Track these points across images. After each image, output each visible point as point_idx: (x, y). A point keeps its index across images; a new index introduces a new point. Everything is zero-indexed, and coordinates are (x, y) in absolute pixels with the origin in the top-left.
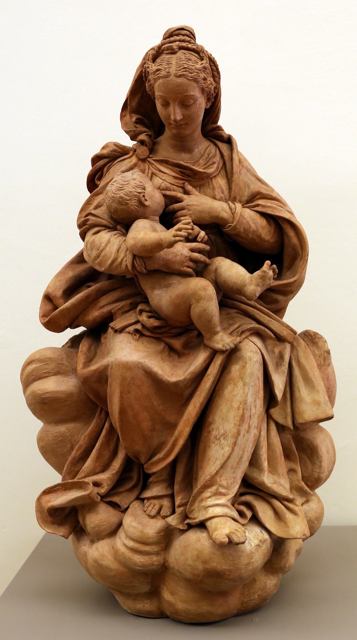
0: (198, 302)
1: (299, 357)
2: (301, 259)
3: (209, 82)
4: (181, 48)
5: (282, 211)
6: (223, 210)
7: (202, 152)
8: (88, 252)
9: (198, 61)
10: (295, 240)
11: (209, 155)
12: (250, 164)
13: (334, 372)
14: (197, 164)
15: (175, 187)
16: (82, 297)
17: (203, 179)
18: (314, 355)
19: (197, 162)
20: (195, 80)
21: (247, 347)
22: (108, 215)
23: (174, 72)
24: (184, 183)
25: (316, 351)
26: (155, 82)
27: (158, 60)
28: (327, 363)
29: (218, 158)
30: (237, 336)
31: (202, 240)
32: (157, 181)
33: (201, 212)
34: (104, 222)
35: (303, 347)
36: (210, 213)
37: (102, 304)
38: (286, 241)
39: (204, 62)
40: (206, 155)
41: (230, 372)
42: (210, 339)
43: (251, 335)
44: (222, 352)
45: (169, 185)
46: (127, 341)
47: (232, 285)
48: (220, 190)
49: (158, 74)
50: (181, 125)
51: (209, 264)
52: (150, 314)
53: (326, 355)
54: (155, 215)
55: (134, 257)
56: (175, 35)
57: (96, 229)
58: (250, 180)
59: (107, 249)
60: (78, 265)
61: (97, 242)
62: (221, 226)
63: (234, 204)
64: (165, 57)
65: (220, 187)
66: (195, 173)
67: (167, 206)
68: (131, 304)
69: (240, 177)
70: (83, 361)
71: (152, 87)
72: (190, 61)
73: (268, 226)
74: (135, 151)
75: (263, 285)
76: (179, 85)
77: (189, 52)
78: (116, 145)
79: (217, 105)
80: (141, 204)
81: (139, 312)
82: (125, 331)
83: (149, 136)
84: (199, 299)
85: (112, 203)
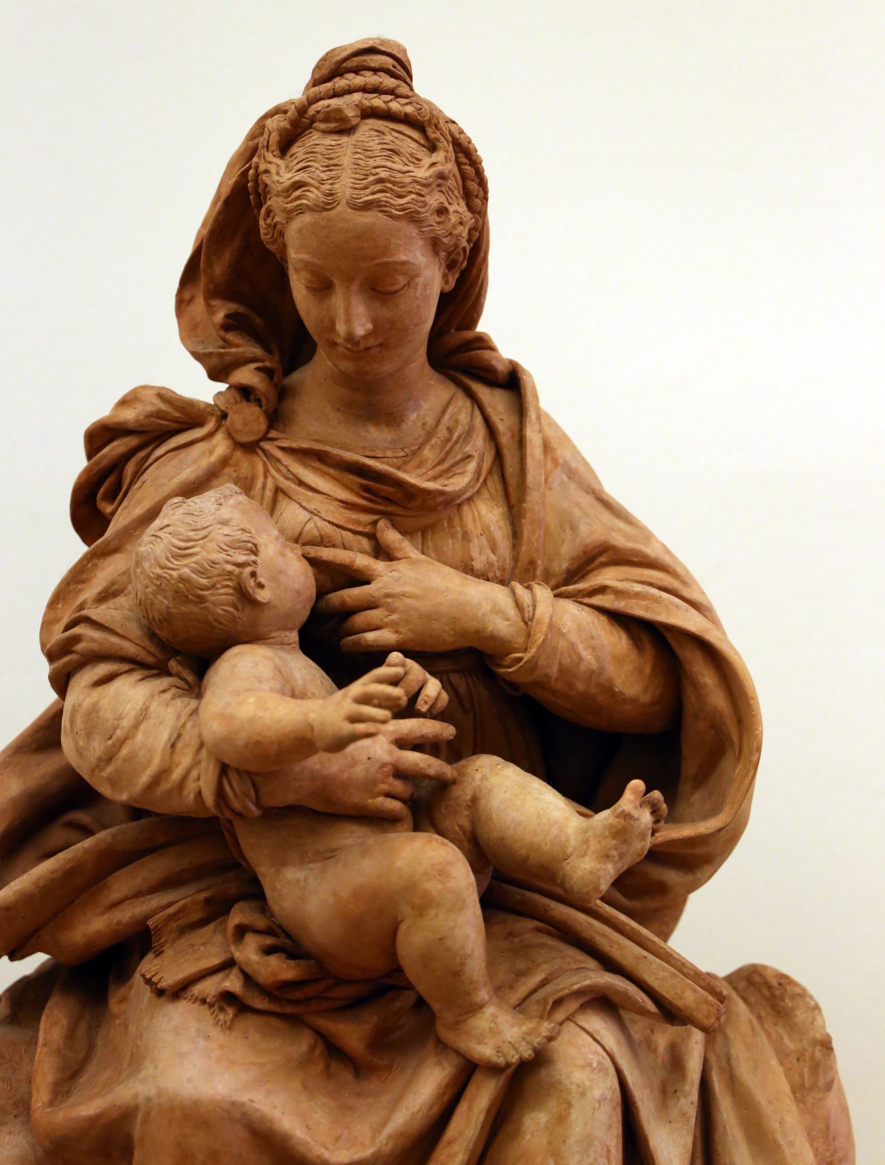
0: (421, 915)
1: (734, 1063)
2: (738, 758)
3: (454, 219)
4: (369, 113)
5: (677, 607)
6: (497, 610)
7: (430, 420)
8: (76, 743)
9: (422, 153)
10: (718, 699)
11: (450, 430)
12: (576, 453)
13: (844, 1109)
14: (414, 463)
15: (348, 535)
16: (53, 872)
17: (433, 509)
18: (782, 1055)
19: (414, 453)
20: (413, 217)
21: (572, 1051)
22: (141, 627)
23: (348, 192)
24: (375, 523)
25: (786, 1040)
26: (289, 220)
27: (298, 150)
28: (822, 1081)
29: (478, 442)
30: (541, 1017)
31: (433, 706)
32: (293, 514)
33: (428, 617)
34: (130, 648)
35: (744, 1027)
36: (455, 620)
37: (115, 896)
38: (690, 698)
39: (439, 156)
40: (442, 432)
41: (517, 1133)
42: (457, 1025)
43: (584, 1007)
44: (493, 1069)
45: (328, 529)
46: (198, 1030)
47: (524, 852)
48: (484, 540)
49: (299, 198)
50: (367, 349)
51: (454, 782)
52: (269, 941)
53: (818, 1054)
54: (286, 629)
55: (224, 769)
56: (350, 71)
57: (103, 669)
58: (578, 504)
59: (140, 736)
60: (38, 757)
61: (107, 714)
62: (491, 657)
63: (529, 587)
64: (317, 140)
65: (486, 531)
66: (409, 493)
67: (321, 593)
68: (207, 901)
69: (546, 496)
70: (50, 1078)
71: (279, 233)
72: (396, 158)
73: (634, 654)
74: (224, 416)
75: (621, 856)
76: (363, 235)
77: (392, 125)
78: (163, 395)
79: (478, 276)
80: (244, 597)
81: (234, 935)
82: (188, 994)
83: (268, 372)
84: (424, 905)
85: (155, 594)
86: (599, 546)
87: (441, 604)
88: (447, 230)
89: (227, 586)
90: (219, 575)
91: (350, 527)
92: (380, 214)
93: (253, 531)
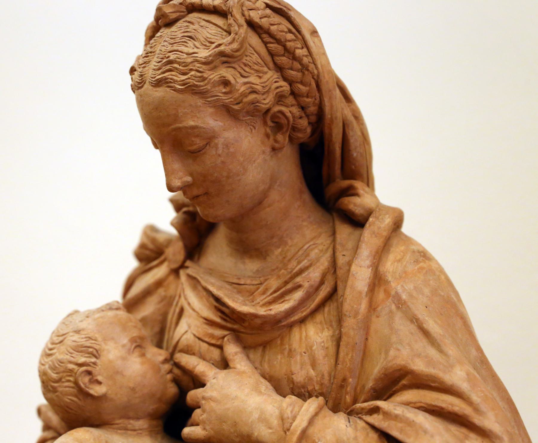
6: (263, 419)
15: (205, 346)
48: (306, 358)
86: (400, 370)
87: (228, 409)
88: (235, 99)
89: (69, 381)
90: (64, 372)
91: (206, 339)
92: (168, 89)
93: (100, 339)
